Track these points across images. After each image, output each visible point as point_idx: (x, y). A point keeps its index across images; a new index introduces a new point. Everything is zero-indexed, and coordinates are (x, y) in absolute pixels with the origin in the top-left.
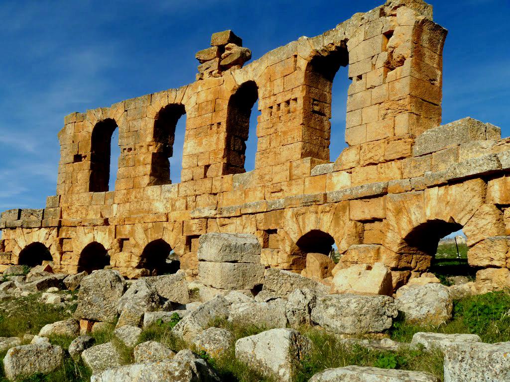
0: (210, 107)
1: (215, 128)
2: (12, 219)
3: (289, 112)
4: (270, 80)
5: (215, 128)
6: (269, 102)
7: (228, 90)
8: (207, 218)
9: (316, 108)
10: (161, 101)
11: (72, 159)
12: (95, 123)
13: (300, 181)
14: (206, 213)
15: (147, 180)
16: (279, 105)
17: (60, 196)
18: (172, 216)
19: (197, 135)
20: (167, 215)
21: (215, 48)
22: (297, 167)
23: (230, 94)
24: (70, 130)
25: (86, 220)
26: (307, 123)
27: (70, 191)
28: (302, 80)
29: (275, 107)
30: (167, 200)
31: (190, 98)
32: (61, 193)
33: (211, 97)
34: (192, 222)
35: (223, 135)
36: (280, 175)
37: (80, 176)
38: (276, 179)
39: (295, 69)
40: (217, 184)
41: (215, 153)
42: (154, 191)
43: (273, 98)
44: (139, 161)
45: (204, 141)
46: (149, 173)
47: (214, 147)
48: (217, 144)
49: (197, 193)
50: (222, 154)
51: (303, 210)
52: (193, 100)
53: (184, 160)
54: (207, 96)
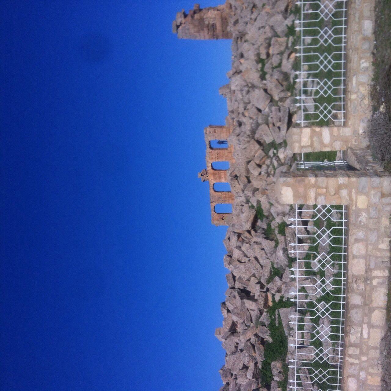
0: (215, 176)
7: (212, 171)
10: (212, 191)
31: (212, 182)
45: (222, 177)
52: (213, 181)
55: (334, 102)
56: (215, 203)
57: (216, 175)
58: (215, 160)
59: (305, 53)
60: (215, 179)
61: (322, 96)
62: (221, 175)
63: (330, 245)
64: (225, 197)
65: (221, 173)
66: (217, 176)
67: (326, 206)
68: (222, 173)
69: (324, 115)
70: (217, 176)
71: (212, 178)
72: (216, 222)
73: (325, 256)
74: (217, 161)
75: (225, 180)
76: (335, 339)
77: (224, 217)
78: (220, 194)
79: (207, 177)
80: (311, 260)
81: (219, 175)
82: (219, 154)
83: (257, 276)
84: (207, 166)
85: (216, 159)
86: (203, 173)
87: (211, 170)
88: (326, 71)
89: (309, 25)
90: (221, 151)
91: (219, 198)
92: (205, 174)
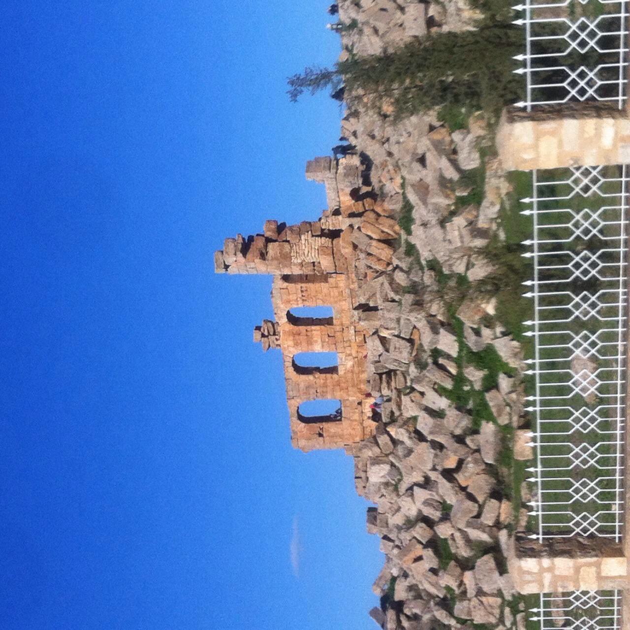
0: (297, 337)
1: (309, 334)
2: (360, 483)
3: (306, 290)
4: (289, 301)
5: (309, 334)
6: (300, 302)
7: (289, 327)
8: (355, 331)
9: (305, 278)
10: (291, 372)
11: (321, 439)
12: (299, 422)
13: (338, 282)
14: (352, 332)
15: (335, 376)
16: (302, 296)
17: (345, 445)
18: (354, 355)
19: (311, 344)
20: (354, 358)
21: (263, 339)
22: (332, 284)
23: (292, 325)
24: (303, 443)
25: (360, 420)
26: (313, 282)
27: (341, 436)
28: (293, 285)
29: (304, 298)
30: (346, 359)
31: (290, 352)
32: (343, 444)
33: (291, 338)
34: (357, 341)
35: (313, 328)
36: (335, 292)
37: (332, 430)
38: (337, 294)
39: (287, 289)
40: (338, 328)
41: (321, 331)
42: (341, 371)
43: (299, 299)
44: (324, 383)
45: (315, 339)
46: (331, 375)
47: (319, 333)
48: (318, 330)
49: (342, 340)
50: (322, 327)
51: (351, 280)
52: (292, 349)
53: (324, 351)
54: (291, 340)
55: (603, 206)
56: (298, 400)
57: (299, 334)
58: (298, 304)
59: (544, 511)
60: (296, 344)
61: (574, 99)
62: (312, 335)
63: (597, 396)
64: (325, 385)
65: (312, 331)
66: (302, 338)
67: (588, 592)
68: (314, 332)
69: (590, 526)
70: (302, 338)
71: (291, 343)
72: (303, 443)
73: (579, 370)
74: (301, 305)
75: (323, 346)
76: (609, 520)
77: (322, 429)
78: (311, 377)
79: (277, 340)
80: (550, 608)
81: (307, 335)
82: (306, 290)
83: (404, 268)
84: (275, 314)
85: (299, 302)
86: (266, 331)
87: (288, 324)
88: (586, 238)
89: (551, 508)
90: (311, 286)
91: (308, 387)
92: (272, 333)
